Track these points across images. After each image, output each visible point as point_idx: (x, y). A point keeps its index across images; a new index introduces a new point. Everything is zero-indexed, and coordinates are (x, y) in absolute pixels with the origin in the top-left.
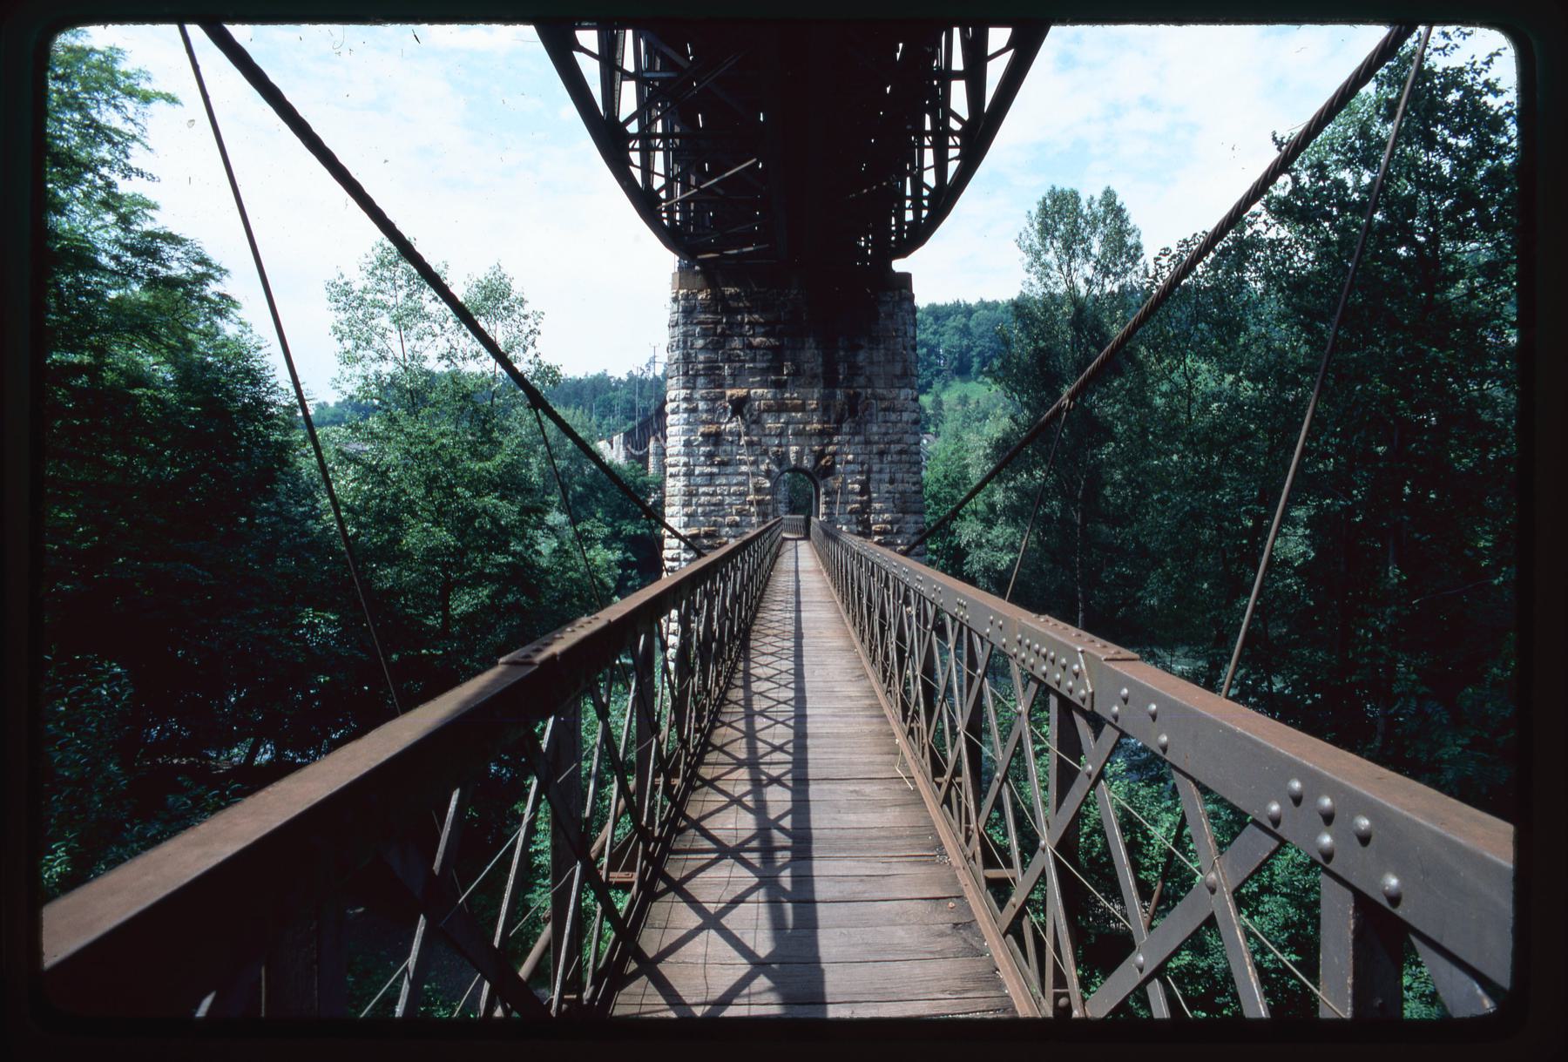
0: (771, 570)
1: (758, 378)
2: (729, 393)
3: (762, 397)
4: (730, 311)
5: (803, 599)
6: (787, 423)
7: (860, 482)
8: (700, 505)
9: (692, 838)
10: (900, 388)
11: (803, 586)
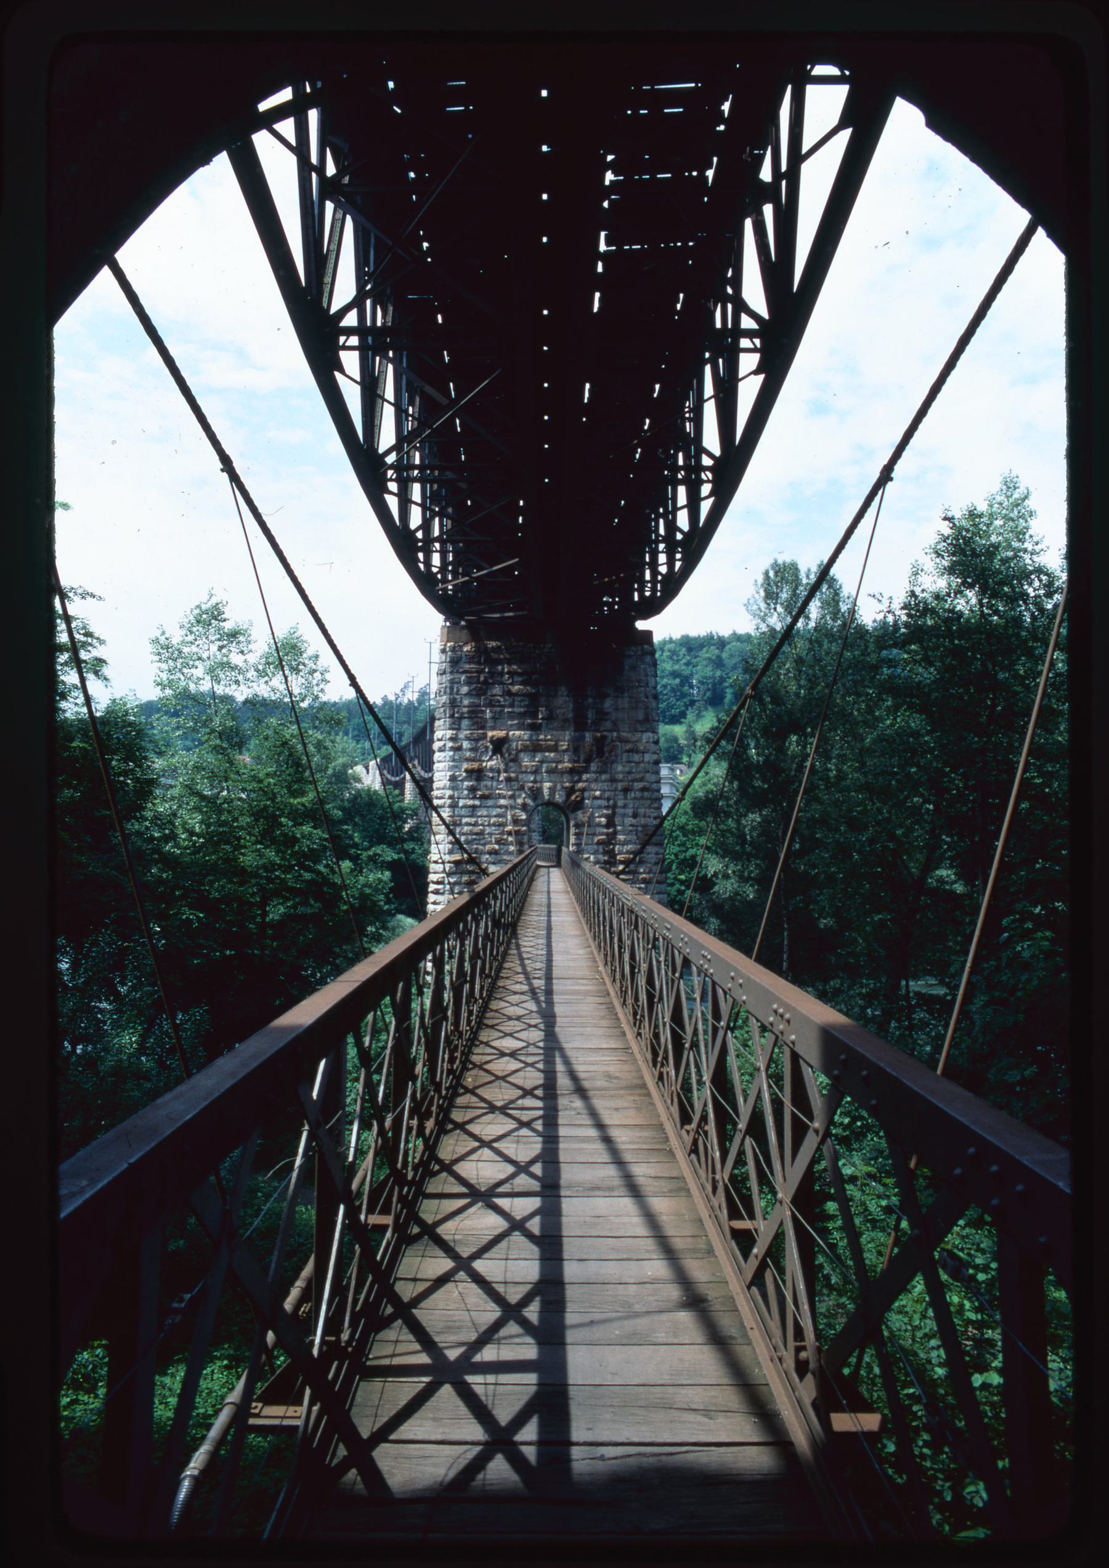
0: (528, 890)
1: (516, 722)
2: (490, 734)
3: (519, 738)
4: (492, 662)
5: (552, 909)
6: (542, 762)
7: (606, 816)
8: (464, 834)
9: (442, 1183)
10: (642, 732)
11: (552, 901)
